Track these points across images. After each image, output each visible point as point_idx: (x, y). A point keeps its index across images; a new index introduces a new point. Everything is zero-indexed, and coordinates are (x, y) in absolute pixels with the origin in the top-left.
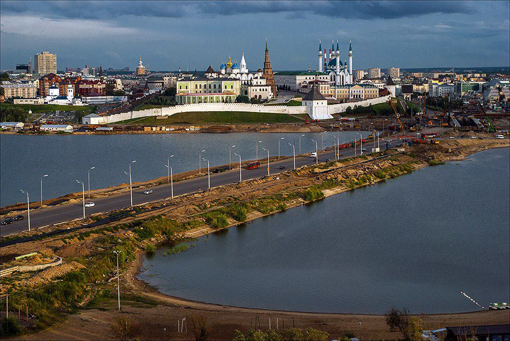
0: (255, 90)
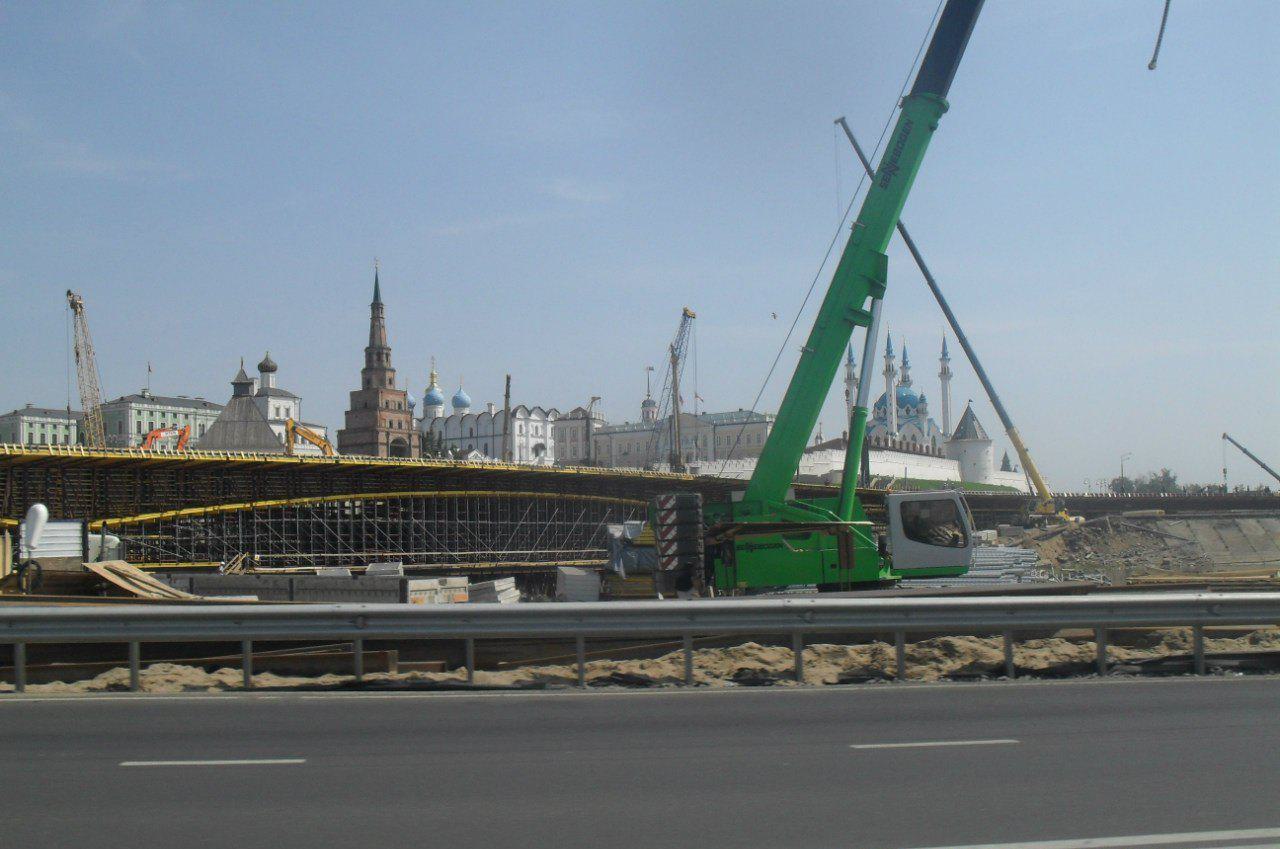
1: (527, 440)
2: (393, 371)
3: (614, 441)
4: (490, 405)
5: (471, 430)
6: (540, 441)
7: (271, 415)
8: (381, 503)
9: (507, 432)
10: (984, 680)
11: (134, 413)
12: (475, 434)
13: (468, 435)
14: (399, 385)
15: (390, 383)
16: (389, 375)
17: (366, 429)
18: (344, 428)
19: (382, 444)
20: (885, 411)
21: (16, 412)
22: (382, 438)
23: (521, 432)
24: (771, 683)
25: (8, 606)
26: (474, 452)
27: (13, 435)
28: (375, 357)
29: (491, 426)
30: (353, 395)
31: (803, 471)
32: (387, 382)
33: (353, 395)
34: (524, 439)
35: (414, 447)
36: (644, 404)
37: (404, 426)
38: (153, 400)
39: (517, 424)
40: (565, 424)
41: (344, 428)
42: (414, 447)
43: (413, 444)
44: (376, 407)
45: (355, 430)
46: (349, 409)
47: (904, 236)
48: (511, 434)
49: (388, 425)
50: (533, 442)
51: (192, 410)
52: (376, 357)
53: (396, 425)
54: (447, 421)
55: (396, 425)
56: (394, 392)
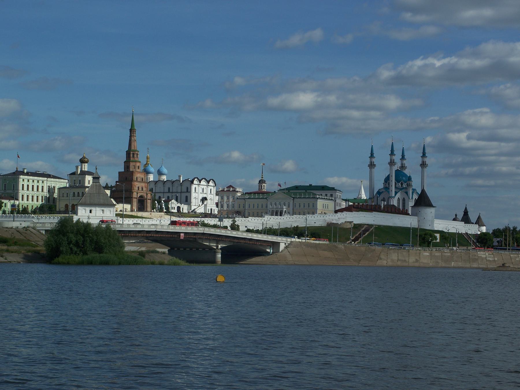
0: (65, 195)
3: (246, 202)
4: (180, 176)
5: (169, 188)
6: (205, 196)
9: (189, 191)
10: (260, 230)
11: (21, 180)
12: (171, 191)
13: (168, 191)
15: (138, 168)
19: (135, 198)
20: (389, 184)
22: (135, 195)
23: (195, 191)
24: (335, 358)
26: (173, 200)
28: (131, 155)
29: (180, 187)
30: (120, 173)
31: (125, 250)
33: (120, 173)
34: (197, 194)
35: (149, 199)
36: (260, 181)
37: (144, 189)
38: (28, 174)
39: (193, 187)
42: (149, 199)
43: (148, 198)
44: (132, 180)
48: (190, 192)
49: (137, 189)
50: (201, 196)
51: (46, 179)
52: (130, 154)
53: (140, 189)
55: (140, 189)
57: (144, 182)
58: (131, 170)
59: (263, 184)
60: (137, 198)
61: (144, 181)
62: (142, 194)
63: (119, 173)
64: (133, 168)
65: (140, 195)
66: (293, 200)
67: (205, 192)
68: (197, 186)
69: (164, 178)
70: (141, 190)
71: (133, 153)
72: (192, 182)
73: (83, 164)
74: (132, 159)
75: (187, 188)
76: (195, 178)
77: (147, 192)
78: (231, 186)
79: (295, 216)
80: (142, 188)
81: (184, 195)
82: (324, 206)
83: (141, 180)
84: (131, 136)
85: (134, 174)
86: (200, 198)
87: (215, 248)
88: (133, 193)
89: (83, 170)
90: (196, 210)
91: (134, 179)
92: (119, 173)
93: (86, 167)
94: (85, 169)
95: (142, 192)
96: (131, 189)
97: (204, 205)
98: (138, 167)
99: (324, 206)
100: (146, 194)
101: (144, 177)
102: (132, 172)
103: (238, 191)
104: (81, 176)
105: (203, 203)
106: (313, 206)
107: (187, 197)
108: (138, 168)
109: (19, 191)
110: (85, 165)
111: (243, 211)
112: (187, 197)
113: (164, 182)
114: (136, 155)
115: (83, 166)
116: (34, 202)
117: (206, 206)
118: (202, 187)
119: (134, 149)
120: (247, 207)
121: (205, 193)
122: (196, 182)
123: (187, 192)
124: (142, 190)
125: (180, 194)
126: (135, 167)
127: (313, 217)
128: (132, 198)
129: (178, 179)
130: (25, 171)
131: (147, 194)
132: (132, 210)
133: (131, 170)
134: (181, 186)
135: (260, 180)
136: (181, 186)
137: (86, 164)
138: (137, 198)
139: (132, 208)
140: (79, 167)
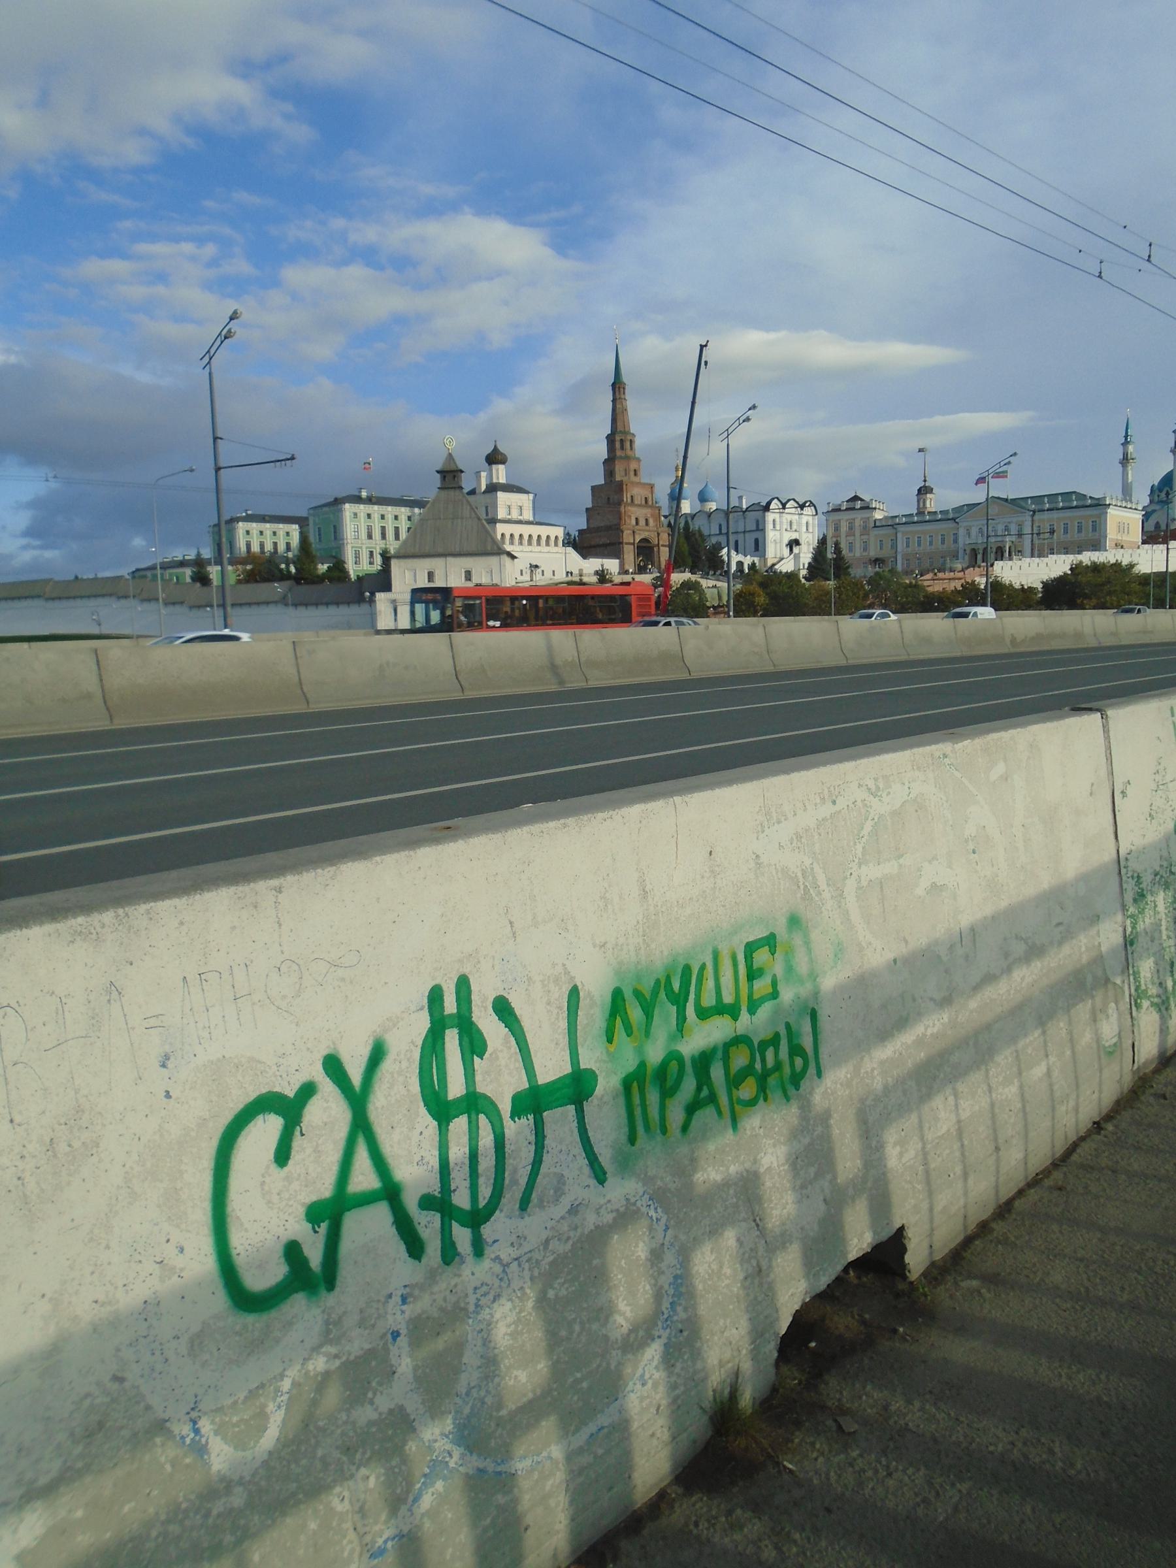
1: (781, 535)
2: (638, 460)
3: (899, 535)
6: (794, 536)
7: (501, 514)
8: (491, 623)
9: (760, 528)
13: (754, 528)
14: (644, 478)
15: (635, 474)
16: (633, 466)
17: (608, 528)
18: (585, 527)
21: (336, 500)
22: (627, 537)
25: (1039, 637)
27: (335, 527)
28: (618, 445)
32: (632, 473)
34: (778, 533)
35: (663, 546)
36: (919, 490)
37: (651, 521)
39: (770, 517)
40: (837, 516)
41: (585, 527)
42: (663, 546)
43: (661, 543)
45: (598, 530)
46: (590, 505)
47: (214, 448)
48: (763, 530)
49: (634, 522)
50: (788, 536)
53: (642, 522)
54: (693, 516)
55: (642, 522)
56: (639, 484)
57: (652, 507)
58: (618, 478)
59: (928, 495)
60: (634, 544)
61: (650, 503)
62: (647, 533)
63: (593, 488)
64: (623, 473)
65: (641, 537)
66: (1033, 516)
67: (794, 527)
68: (777, 516)
69: (712, 506)
70: (644, 524)
71: (621, 440)
72: (767, 508)
73: (494, 467)
74: (619, 453)
75: (757, 522)
76: (773, 499)
77: (660, 530)
78: (856, 498)
79: (1054, 557)
80: (646, 520)
81: (750, 538)
82: (1126, 530)
83: (643, 502)
84: (614, 401)
85: (624, 486)
86: (786, 541)
87: (443, 1409)
88: (622, 532)
89: (495, 481)
90: (776, 567)
91: (625, 500)
92: (593, 488)
93: (500, 474)
94: (498, 478)
95: (647, 528)
96: (619, 524)
97: (792, 556)
98: (635, 470)
99: (1126, 530)
100: (656, 533)
101: (650, 495)
102: (621, 484)
103: (875, 508)
104: (487, 495)
105: (791, 550)
106: (1094, 529)
107: (757, 541)
108: (635, 474)
109: (345, 541)
110: (497, 470)
111: (891, 557)
112: (757, 541)
113: (709, 515)
114: (628, 443)
115: (494, 471)
116: (361, 566)
117: (797, 557)
118: (789, 517)
119: (622, 430)
120: (901, 546)
121: (796, 531)
122: (775, 505)
123: (758, 529)
124: (647, 524)
125: (742, 535)
126: (626, 472)
127: (1043, 565)
128: (622, 543)
129: (737, 505)
130: (364, 494)
131: (658, 534)
132: (624, 571)
133: (618, 478)
134: (745, 518)
135: (921, 488)
136: (745, 518)
137: (501, 467)
138: (634, 544)
139: (622, 565)
140: (483, 474)
